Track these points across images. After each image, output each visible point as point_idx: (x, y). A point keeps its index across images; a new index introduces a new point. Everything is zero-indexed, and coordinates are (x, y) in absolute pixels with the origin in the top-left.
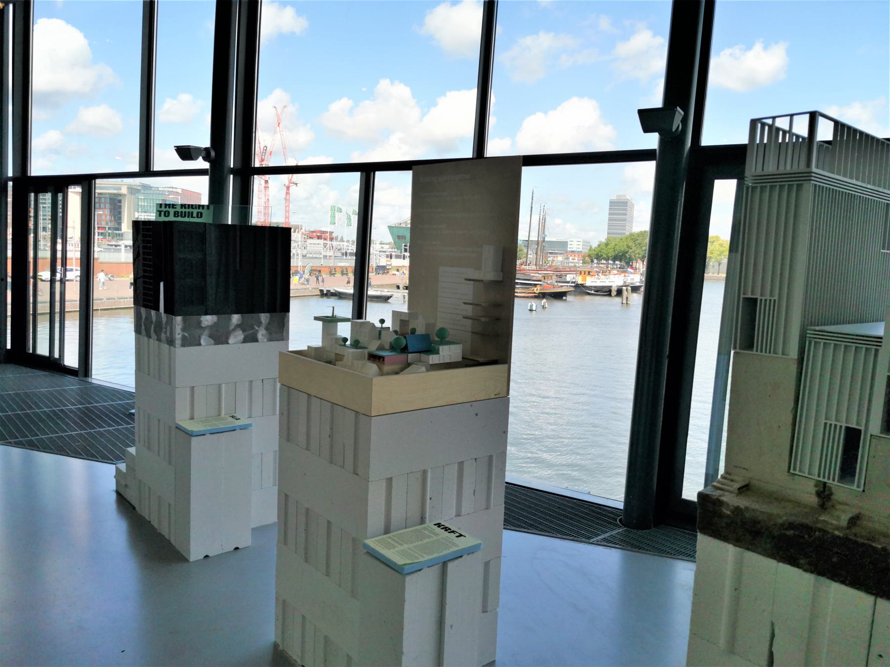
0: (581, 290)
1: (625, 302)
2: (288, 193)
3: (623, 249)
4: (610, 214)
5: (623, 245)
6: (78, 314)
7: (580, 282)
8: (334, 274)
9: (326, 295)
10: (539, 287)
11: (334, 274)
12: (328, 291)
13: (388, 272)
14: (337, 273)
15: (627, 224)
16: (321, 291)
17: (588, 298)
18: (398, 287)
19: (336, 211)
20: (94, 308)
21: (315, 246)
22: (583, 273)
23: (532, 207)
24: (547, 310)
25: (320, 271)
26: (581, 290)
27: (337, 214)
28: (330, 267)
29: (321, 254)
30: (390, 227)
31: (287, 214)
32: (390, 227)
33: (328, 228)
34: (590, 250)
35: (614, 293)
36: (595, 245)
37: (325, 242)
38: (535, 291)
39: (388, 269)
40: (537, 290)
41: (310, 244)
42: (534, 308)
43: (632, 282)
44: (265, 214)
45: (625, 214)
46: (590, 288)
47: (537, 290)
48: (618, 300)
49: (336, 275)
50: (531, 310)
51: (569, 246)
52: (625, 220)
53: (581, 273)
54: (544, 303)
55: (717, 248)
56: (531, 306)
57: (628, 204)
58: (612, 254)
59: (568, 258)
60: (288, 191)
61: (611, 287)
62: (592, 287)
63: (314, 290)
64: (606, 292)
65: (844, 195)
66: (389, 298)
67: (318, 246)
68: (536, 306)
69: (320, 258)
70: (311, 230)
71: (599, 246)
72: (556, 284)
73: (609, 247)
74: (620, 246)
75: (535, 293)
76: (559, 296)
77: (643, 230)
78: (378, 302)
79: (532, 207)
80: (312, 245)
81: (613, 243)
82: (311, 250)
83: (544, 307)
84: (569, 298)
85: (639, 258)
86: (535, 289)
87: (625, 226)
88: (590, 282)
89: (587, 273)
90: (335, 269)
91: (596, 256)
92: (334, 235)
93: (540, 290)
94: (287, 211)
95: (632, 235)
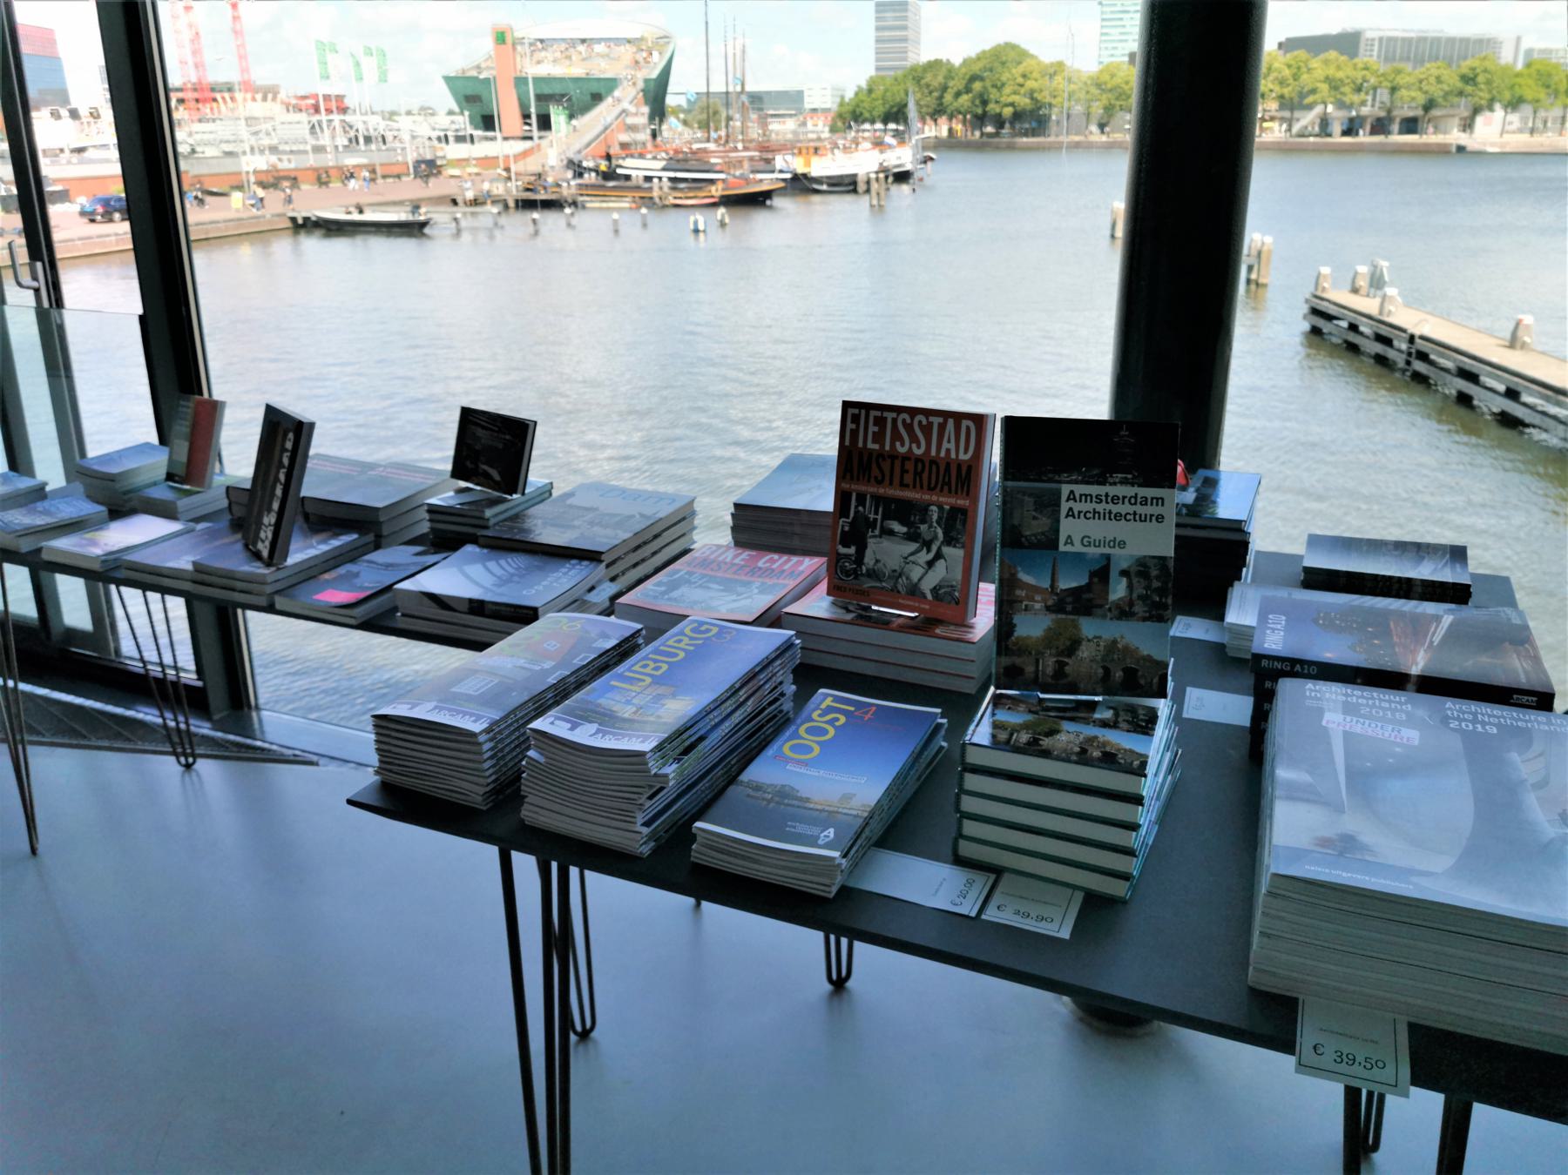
0: (801, 185)
1: (875, 202)
2: (236, 18)
3: (898, 100)
4: (878, 29)
5: (898, 91)
6: (132, 255)
7: (800, 170)
8: (326, 184)
9: (304, 226)
10: (720, 186)
11: (326, 184)
12: (306, 219)
13: (439, 173)
14: (332, 179)
15: (910, 48)
16: (293, 220)
17: (816, 198)
18: (455, 202)
19: (327, 51)
20: (192, 237)
21: (291, 126)
22: (804, 151)
23: (707, 23)
24: (728, 228)
25: (295, 179)
26: (801, 185)
27: (330, 57)
28: (315, 170)
29: (306, 143)
30: (448, 79)
31: (244, 64)
32: (448, 79)
33: (323, 89)
34: (842, 104)
35: (861, 187)
36: (849, 95)
37: (315, 119)
38: (714, 193)
39: (441, 166)
40: (716, 191)
41: (283, 123)
42: (701, 227)
43: (898, 162)
44: (197, 66)
45: (905, 28)
46: (818, 180)
47: (717, 190)
48: (866, 198)
49: (331, 185)
50: (696, 231)
51: (806, 99)
52: (905, 40)
53: (800, 153)
54: (723, 215)
55: (686, 136)
56: (696, 223)
57: (910, 7)
58: (880, 110)
59: (804, 124)
60: (236, 14)
61: (855, 176)
62: (822, 177)
63: (276, 219)
64: (847, 185)
65: (887, 33)
66: (423, 225)
67: (298, 126)
68: (705, 223)
69: (305, 152)
70: (300, 95)
71: (857, 94)
72: (751, 176)
73: (873, 96)
74: (893, 95)
75: (712, 197)
76: (758, 200)
77: (932, 59)
78: (401, 235)
79: (707, 23)
80: (285, 126)
81: (882, 88)
82: (285, 137)
83: (723, 224)
84: (777, 201)
85: (928, 114)
86: (713, 188)
87: (906, 52)
88: (820, 167)
89: (812, 151)
90: (327, 172)
91: (851, 117)
92: (348, 102)
93: (723, 189)
94: (242, 57)
95: (913, 69)
